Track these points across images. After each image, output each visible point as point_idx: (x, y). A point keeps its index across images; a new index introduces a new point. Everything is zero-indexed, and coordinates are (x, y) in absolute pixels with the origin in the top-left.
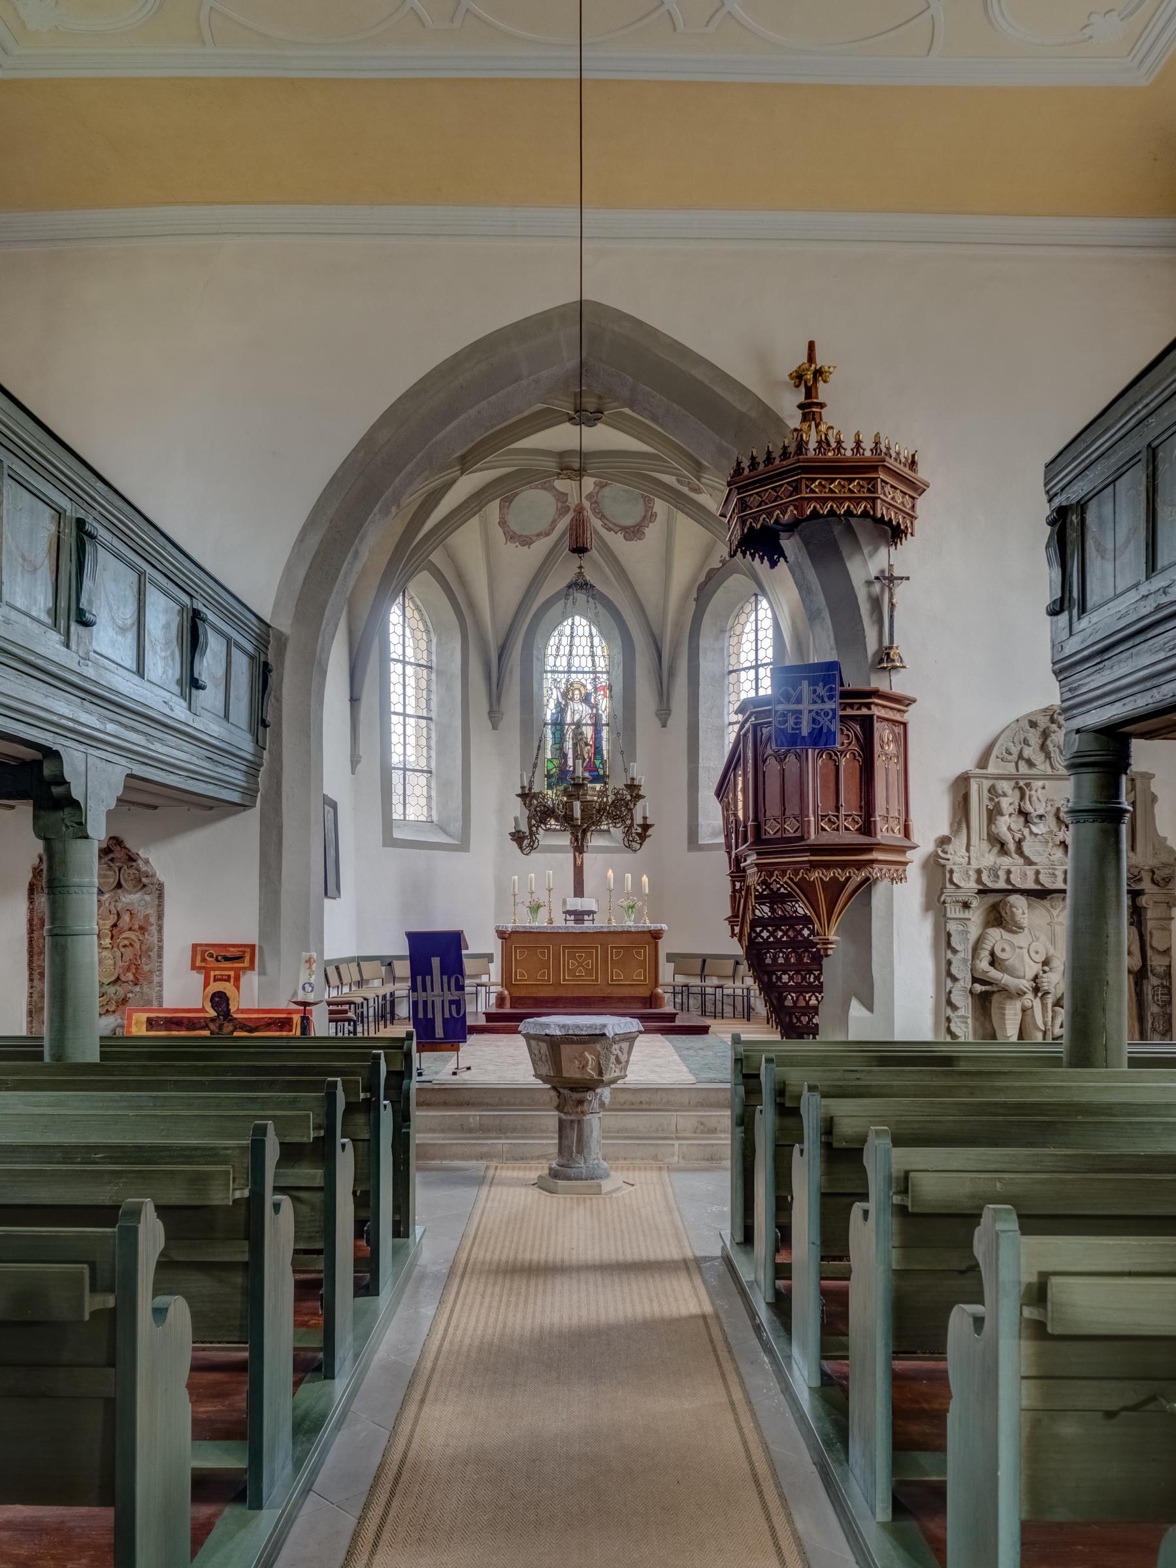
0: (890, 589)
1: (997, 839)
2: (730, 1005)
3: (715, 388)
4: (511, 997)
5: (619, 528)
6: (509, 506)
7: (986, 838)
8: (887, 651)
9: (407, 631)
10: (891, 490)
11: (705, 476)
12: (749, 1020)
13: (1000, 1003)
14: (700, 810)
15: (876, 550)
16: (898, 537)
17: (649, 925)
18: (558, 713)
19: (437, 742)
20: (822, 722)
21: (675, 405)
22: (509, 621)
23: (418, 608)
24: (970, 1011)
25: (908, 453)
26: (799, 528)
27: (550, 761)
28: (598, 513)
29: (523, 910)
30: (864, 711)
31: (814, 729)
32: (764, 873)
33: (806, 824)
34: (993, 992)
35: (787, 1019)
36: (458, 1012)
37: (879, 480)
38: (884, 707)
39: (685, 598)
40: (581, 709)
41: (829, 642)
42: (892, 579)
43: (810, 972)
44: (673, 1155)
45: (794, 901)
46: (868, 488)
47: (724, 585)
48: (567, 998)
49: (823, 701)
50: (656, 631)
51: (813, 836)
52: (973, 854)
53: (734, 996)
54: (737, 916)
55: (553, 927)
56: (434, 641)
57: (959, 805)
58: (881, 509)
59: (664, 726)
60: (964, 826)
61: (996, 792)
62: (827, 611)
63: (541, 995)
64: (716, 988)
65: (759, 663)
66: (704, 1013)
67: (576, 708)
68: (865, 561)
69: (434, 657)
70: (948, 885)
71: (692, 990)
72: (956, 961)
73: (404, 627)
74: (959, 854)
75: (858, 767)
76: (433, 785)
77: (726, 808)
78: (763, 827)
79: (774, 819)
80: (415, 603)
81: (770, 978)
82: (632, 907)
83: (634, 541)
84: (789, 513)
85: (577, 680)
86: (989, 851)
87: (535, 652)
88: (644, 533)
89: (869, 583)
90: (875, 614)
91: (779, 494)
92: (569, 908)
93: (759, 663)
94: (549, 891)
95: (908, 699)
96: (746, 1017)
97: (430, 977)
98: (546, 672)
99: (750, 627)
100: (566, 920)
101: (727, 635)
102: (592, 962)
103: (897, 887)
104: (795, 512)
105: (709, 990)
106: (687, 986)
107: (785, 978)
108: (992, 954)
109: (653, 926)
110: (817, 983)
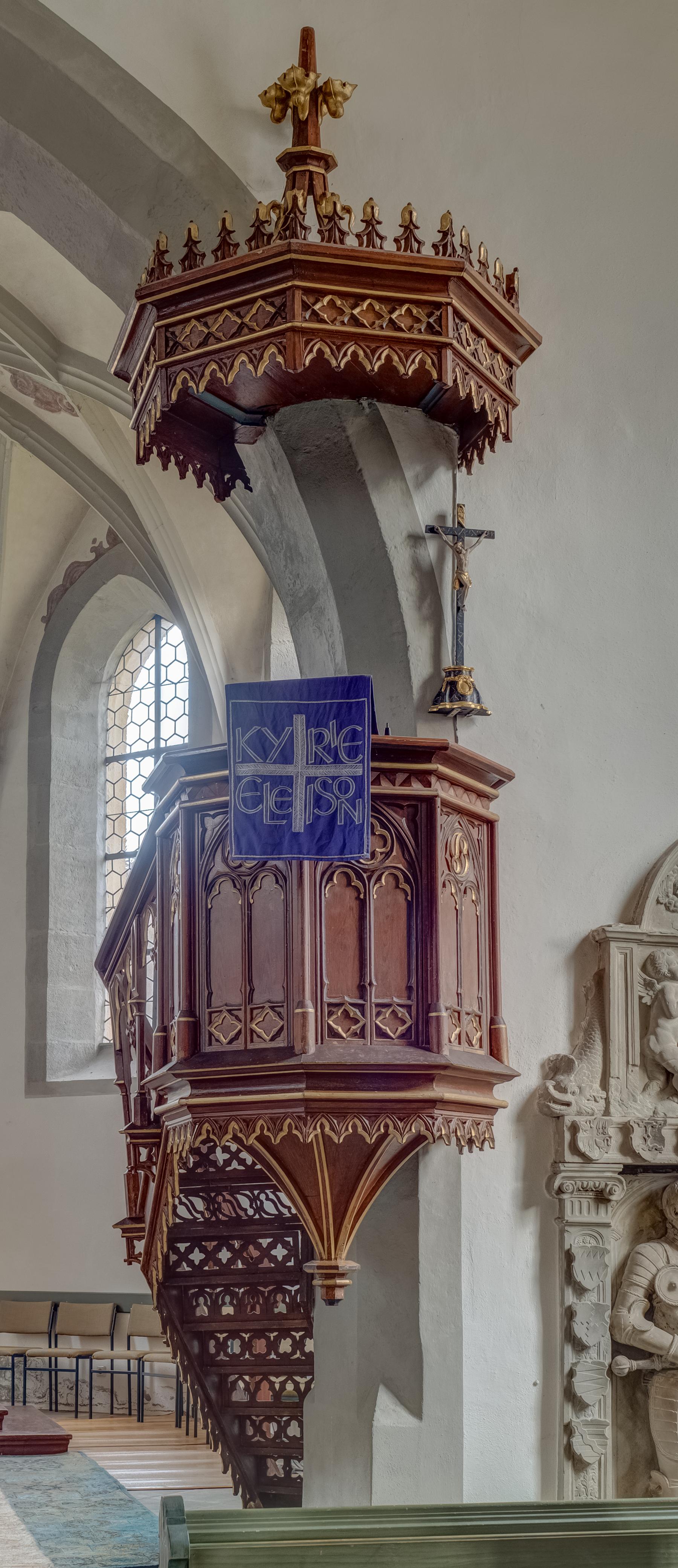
0: (457, 552)
1: (658, 1065)
2: (104, 1390)
3: (108, 105)
7: (638, 1062)
8: (452, 678)
10: (471, 336)
11: (69, 368)
12: (140, 1419)
13: (666, 1395)
15: (428, 474)
16: (475, 446)
20: (334, 803)
21: (23, 136)
24: (609, 1411)
25: (502, 269)
26: (277, 417)
30: (417, 788)
31: (318, 818)
32: (206, 1126)
33: (298, 1022)
34: (653, 1372)
35: (236, 1429)
37: (450, 309)
38: (454, 783)
41: (334, 659)
42: (459, 533)
43: (285, 1333)
45: (256, 1187)
46: (429, 324)
47: (99, 594)
49: (337, 760)
51: (312, 1048)
52: (614, 1094)
54: (140, 1219)
57: (586, 996)
58: (454, 371)
60: (597, 1037)
61: (657, 971)
62: (330, 592)
64: (78, 1357)
66: (54, 1407)
68: (408, 494)
70: (568, 1156)
71: (32, 1363)
72: (583, 1307)
74: (588, 1093)
75: (404, 904)
77: (119, 995)
78: (205, 1029)
79: (229, 1011)
81: (204, 1347)
84: (266, 362)
86: (644, 1090)
89: (415, 539)
90: (428, 601)
91: (247, 320)
93: (163, 744)
95: (498, 771)
96: (134, 1412)
99: (144, 678)
101: (103, 689)
103: (470, 1159)
104: (280, 359)
105: (65, 1363)
106: (22, 1355)
107: (235, 1347)
108: (651, 1294)
110: (298, 1355)
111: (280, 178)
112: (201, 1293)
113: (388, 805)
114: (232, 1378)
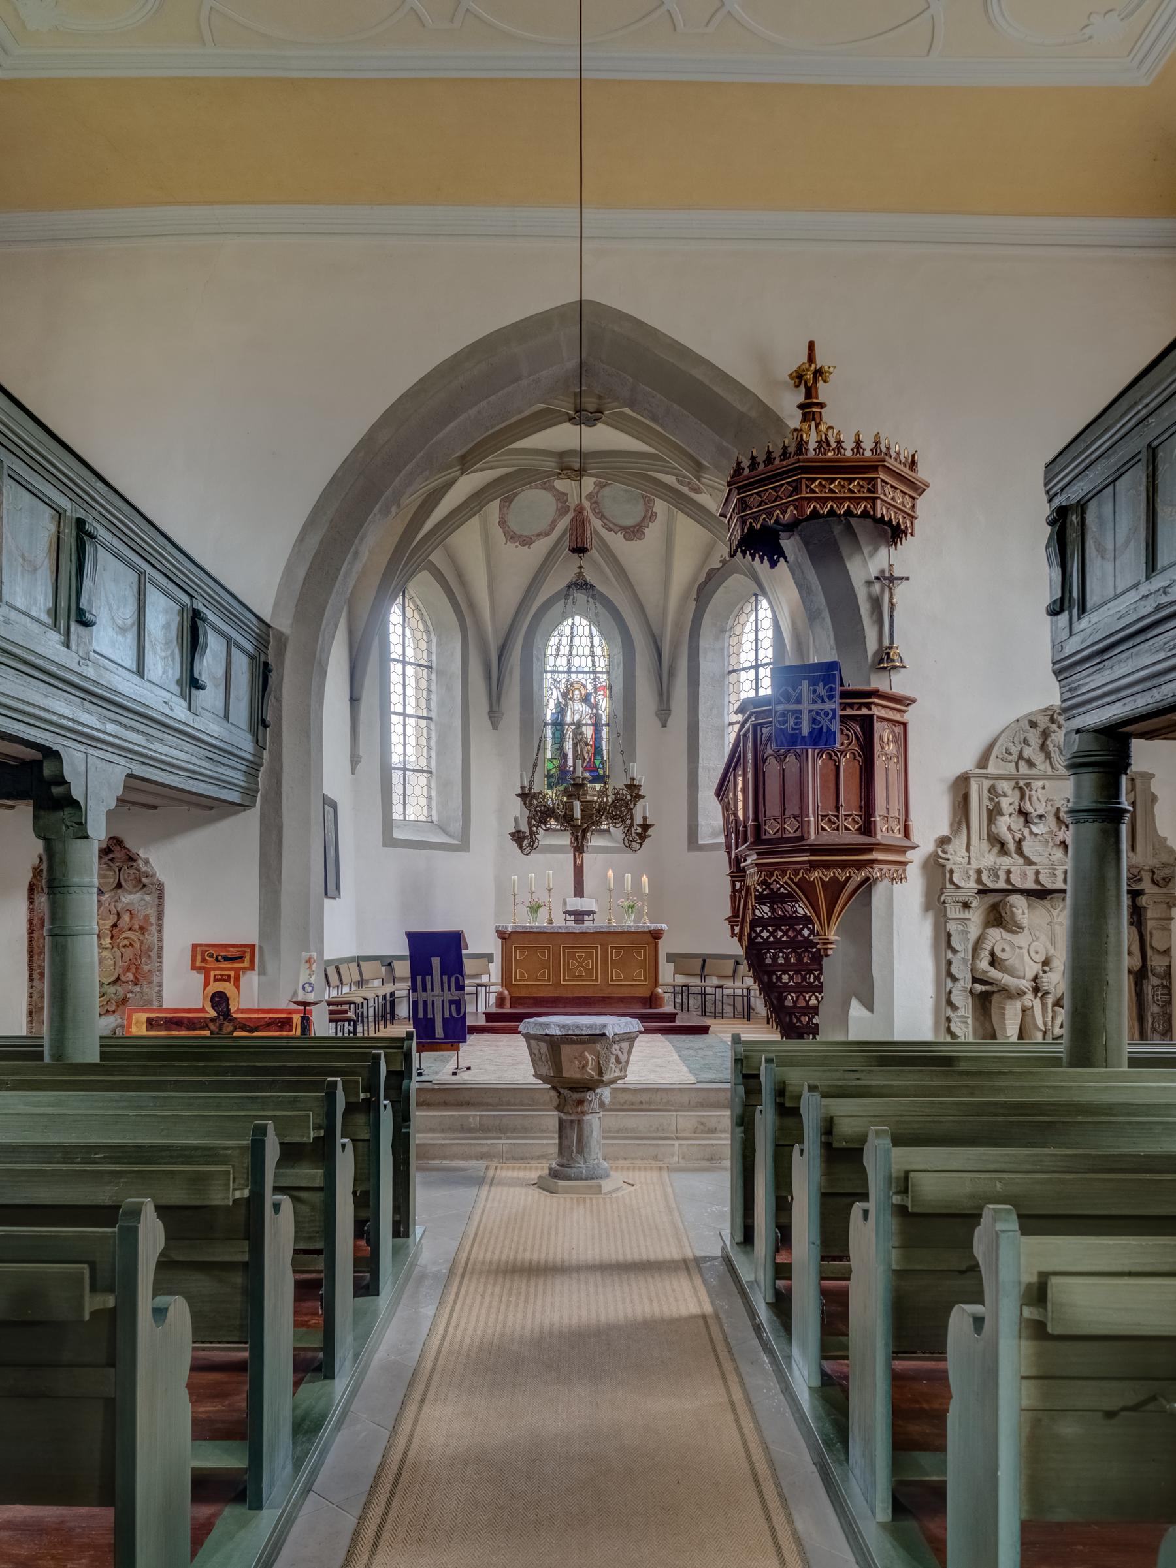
0: (890, 589)
1: (997, 839)
2: (730, 1005)
3: (715, 388)
4: (511, 997)
6: (509, 506)
7: (986, 838)
8: (887, 651)
9: (407, 631)
10: (891, 490)
11: (705, 476)
12: (749, 1020)
13: (1000, 1003)
14: (700, 810)
15: (876, 550)
16: (898, 537)
17: (649, 925)
18: (558, 713)
19: (437, 742)
20: (822, 722)
21: (675, 405)
22: (509, 621)
23: (418, 608)
24: (970, 1011)
25: (908, 453)
26: (799, 528)
27: (550, 761)
28: (598, 513)
29: (523, 910)
30: (864, 711)
31: (814, 729)
32: (764, 873)
33: (806, 824)
34: (993, 992)
35: (787, 1019)
36: (458, 1012)
37: (879, 480)
38: (884, 707)
39: (685, 598)
40: (581, 709)
41: (829, 642)
42: (892, 579)
43: (810, 972)
44: (673, 1155)
46: (868, 488)
47: (724, 585)
48: (567, 998)
49: (823, 701)
50: (656, 631)
51: (813, 836)
52: (973, 854)
53: (734, 996)
54: (737, 916)
55: (553, 927)
56: (434, 641)
57: (959, 805)
58: (881, 509)
59: (664, 726)
60: (964, 826)
61: (996, 792)
62: (827, 611)
63: (541, 995)
64: (716, 988)
65: (759, 663)
66: (704, 1013)
67: (576, 708)
68: (865, 561)
69: (434, 657)
70: (948, 885)
71: (692, 990)
72: (956, 961)
73: (404, 627)
74: (959, 854)
75: (858, 767)
76: (433, 785)
77: (726, 808)
78: (763, 827)
79: (774, 819)
80: (415, 603)
81: (770, 978)
82: (632, 907)
83: (634, 541)
84: (789, 513)
85: (577, 680)
86: (989, 851)
87: (535, 652)
88: (644, 533)
89: (869, 583)
90: (875, 614)
91: (779, 494)
92: (569, 908)
93: (759, 663)
94: (549, 891)
95: (908, 699)
96: (746, 1017)
97: (430, 977)
98: (546, 672)
99: (750, 627)
100: (566, 920)
101: (727, 635)
102: (592, 962)
103: (897, 887)
104: (795, 512)
105: (709, 990)
106: (687, 986)
107: (785, 978)
108: (992, 954)
109: (653, 926)
110: (817, 983)
111: (799, 413)
113: (850, 720)
114: (785, 994)
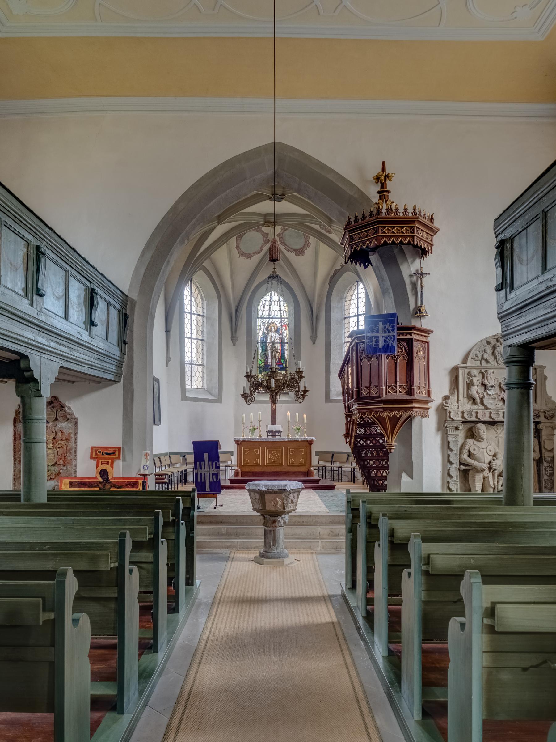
0: (421, 279)
1: (471, 397)
2: (345, 475)
3: (338, 184)
4: (242, 472)
5: (293, 250)
6: (241, 239)
7: (466, 396)
8: (420, 308)
9: (193, 298)
10: (421, 232)
11: (333, 225)
12: (354, 483)
13: (473, 475)
14: (331, 383)
15: (414, 260)
16: (425, 254)
17: (307, 438)
18: (264, 337)
19: (207, 351)
20: (389, 341)
21: (319, 192)
22: (241, 294)
23: (197, 288)
24: (459, 478)
25: (429, 214)
26: (378, 250)
27: (260, 360)
28: (283, 243)
29: (247, 431)
30: (409, 337)
31: (385, 345)
32: (361, 413)
33: (381, 390)
34: (470, 470)
35: (372, 482)
36: (217, 479)
37: (416, 227)
38: (418, 334)
39: (324, 283)
40: (275, 336)
41: (392, 304)
42: (422, 274)
43: (383, 460)
44: (318, 547)
45: (375, 426)
46: (411, 231)
47: (342, 277)
48: (268, 472)
49: (389, 332)
50: (310, 299)
51: (384, 396)
52: (460, 404)
53: (347, 471)
54: (349, 434)
55: (262, 439)
56: (205, 303)
57: (453, 381)
58: (417, 241)
59: (314, 343)
60: (456, 391)
61: (471, 375)
62: (391, 289)
63: (256, 471)
64: (338, 467)
65: (359, 314)
67: (272, 335)
68: (409, 266)
69: (205, 311)
70: (448, 419)
71: (327, 468)
72: (452, 455)
73: (191, 297)
74: (453, 404)
75: (406, 363)
76: (205, 371)
77: (343, 382)
78: (361, 391)
79: (366, 388)
80: (196, 285)
81: (364, 463)
82: (299, 429)
83: (300, 256)
84: (373, 243)
85: (273, 322)
86: (468, 403)
87: (253, 309)
88: (304, 252)
89: (411, 276)
90: (414, 290)
91: (368, 234)
92: (269, 430)
93: (359, 314)
94: (260, 421)
95: (429, 331)
96: (353, 481)
97: (203, 462)
98: (258, 318)
99: (354, 297)
100: (267, 435)
101: (344, 300)
102: (280, 455)
103: (424, 420)
104: (376, 242)
105: (335, 469)
106: (325, 466)
107: (371, 463)
108: (469, 451)
109: (309, 438)
110: (386, 465)
112: (363, 451)
113: (402, 341)
114: (371, 470)
